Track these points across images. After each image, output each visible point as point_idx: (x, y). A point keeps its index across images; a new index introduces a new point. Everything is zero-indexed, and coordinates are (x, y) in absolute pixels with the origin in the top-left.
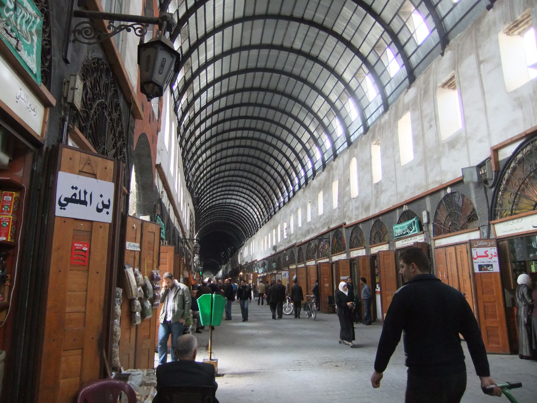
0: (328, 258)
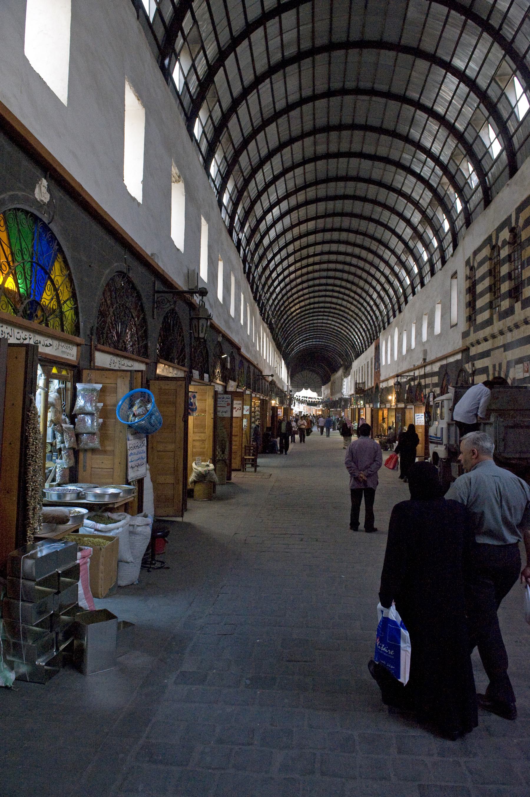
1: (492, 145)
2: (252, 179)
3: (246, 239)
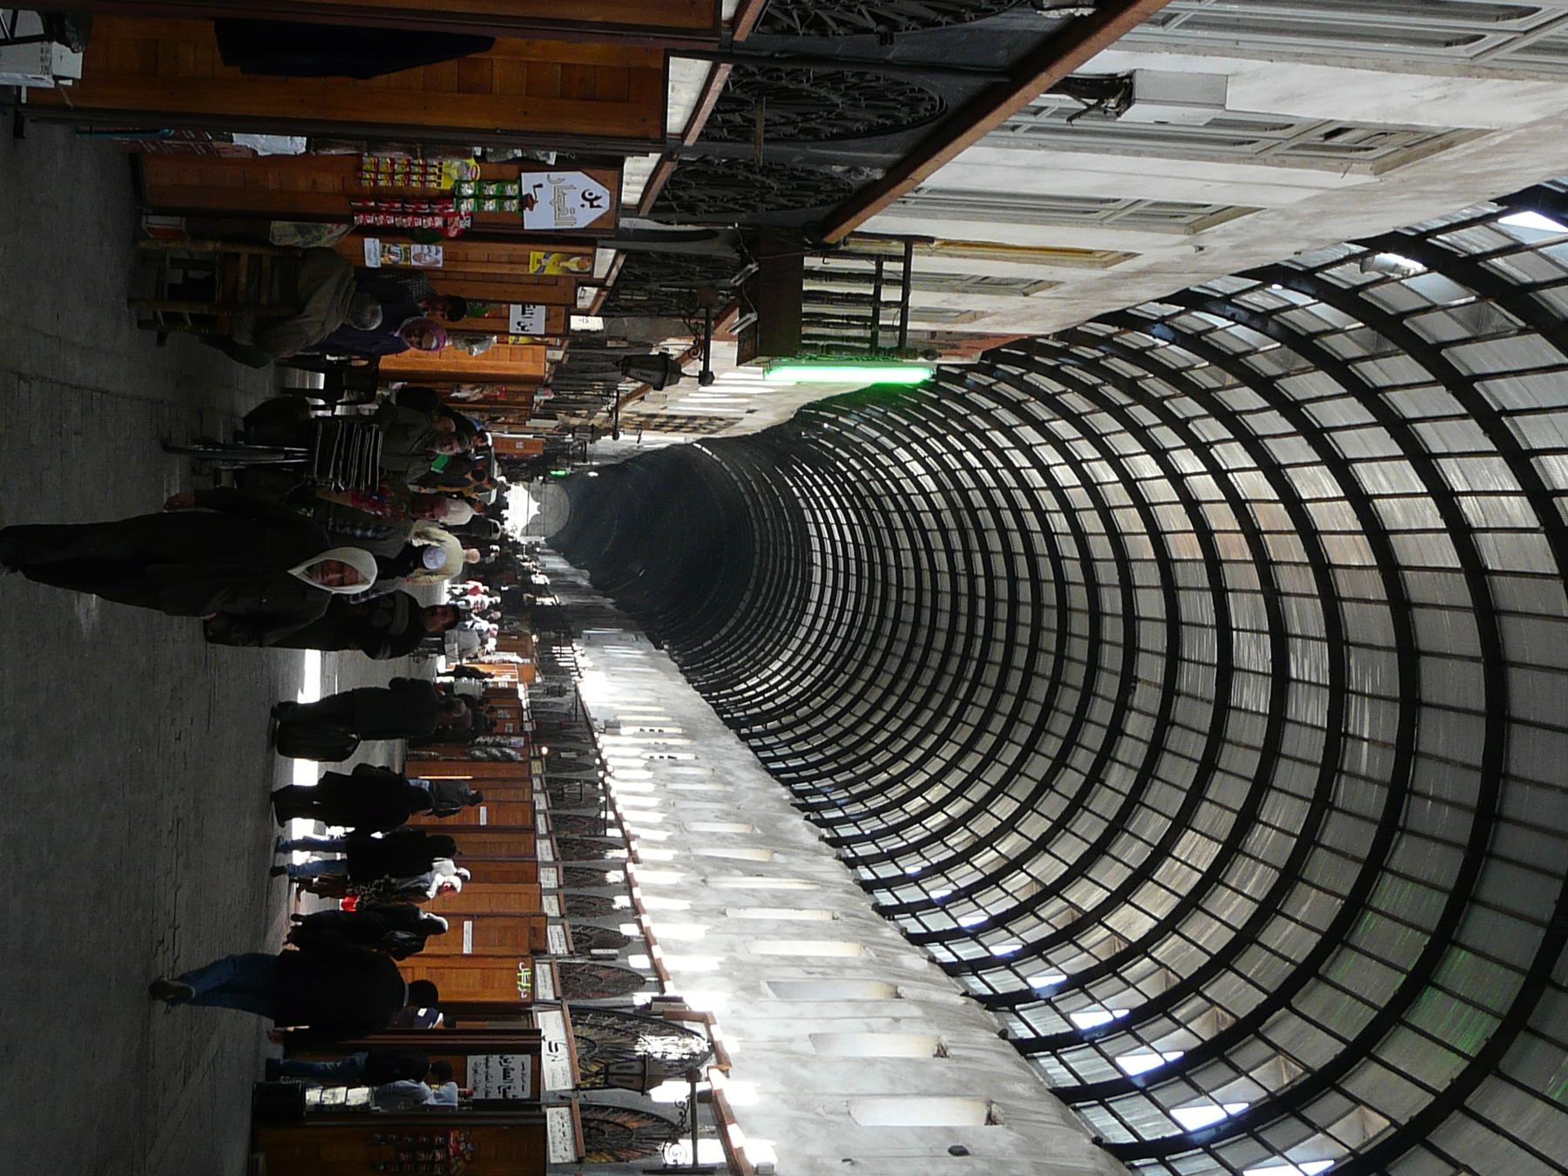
1: (1291, 1167)
3: (1200, 333)
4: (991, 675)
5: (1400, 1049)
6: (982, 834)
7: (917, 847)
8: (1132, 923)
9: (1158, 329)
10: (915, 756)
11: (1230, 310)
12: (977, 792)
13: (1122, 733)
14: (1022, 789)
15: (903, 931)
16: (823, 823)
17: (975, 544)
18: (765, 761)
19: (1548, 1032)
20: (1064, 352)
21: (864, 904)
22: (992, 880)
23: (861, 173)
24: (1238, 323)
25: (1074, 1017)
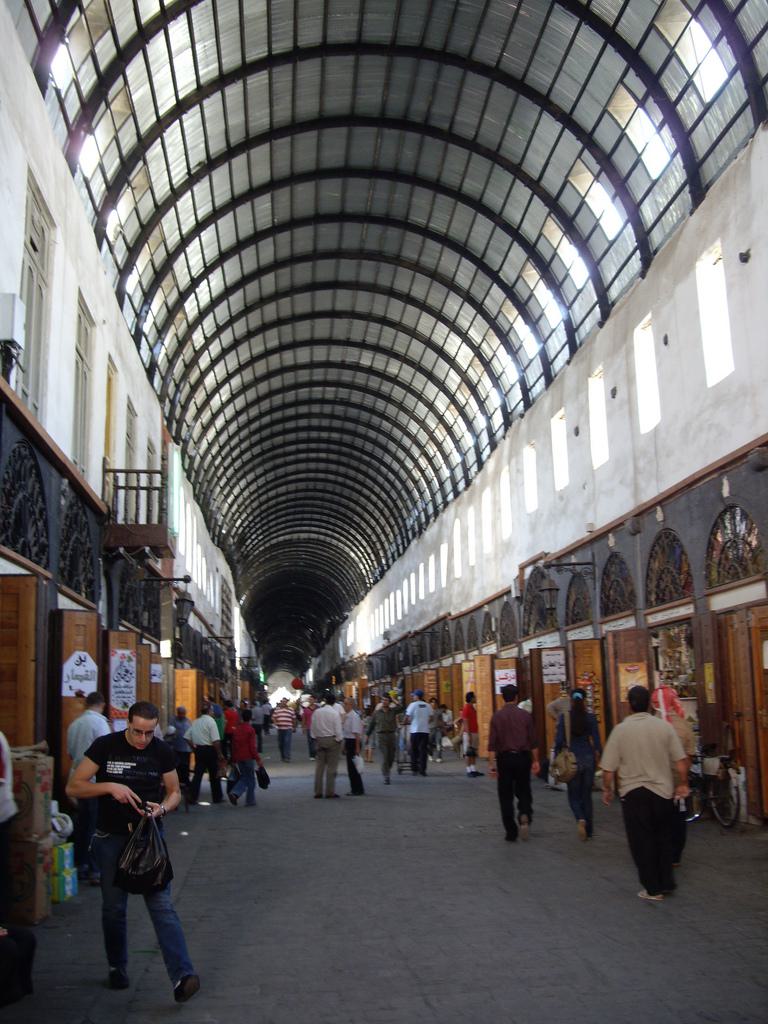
0: (478, 649)
2: (179, 254)
4: (347, 438)
5: (513, 214)
6: (427, 437)
7: (436, 471)
8: (464, 356)
9: (156, 351)
10: (391, 477)
11: (143, 314)
12: (407, 442)
13: (371, 367)
14: (403, 418)
15: (476, 473)
16: (427, 522)
17: (280, 451)
18: (399, 555)
19: (498, 140)
20: (172, 402)
21: (465, 494)
22: (449, 430)
23: (65, 490)
24: (150, 308)
25: (472, 329)
